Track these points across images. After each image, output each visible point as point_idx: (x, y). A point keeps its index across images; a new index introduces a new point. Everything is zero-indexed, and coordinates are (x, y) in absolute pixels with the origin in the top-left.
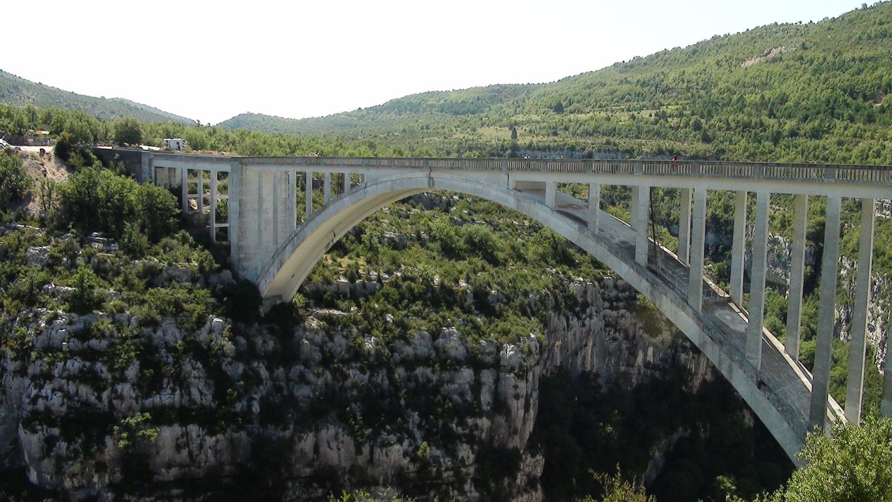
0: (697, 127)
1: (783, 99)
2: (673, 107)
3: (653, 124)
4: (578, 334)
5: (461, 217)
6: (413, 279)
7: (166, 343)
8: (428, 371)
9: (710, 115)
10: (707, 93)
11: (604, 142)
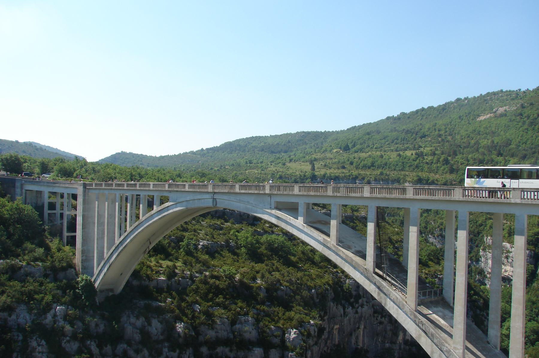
0: (446, 162)
1: (508, 143)
2: (429, 149)
3: (414, 160)
4: (352, 320)
5: (263, 229)
6: (217, 278)
7: (19, 325)
8: (227, 350)
9: (455, 154)
10: (452, 139)
11: (379, 174)
